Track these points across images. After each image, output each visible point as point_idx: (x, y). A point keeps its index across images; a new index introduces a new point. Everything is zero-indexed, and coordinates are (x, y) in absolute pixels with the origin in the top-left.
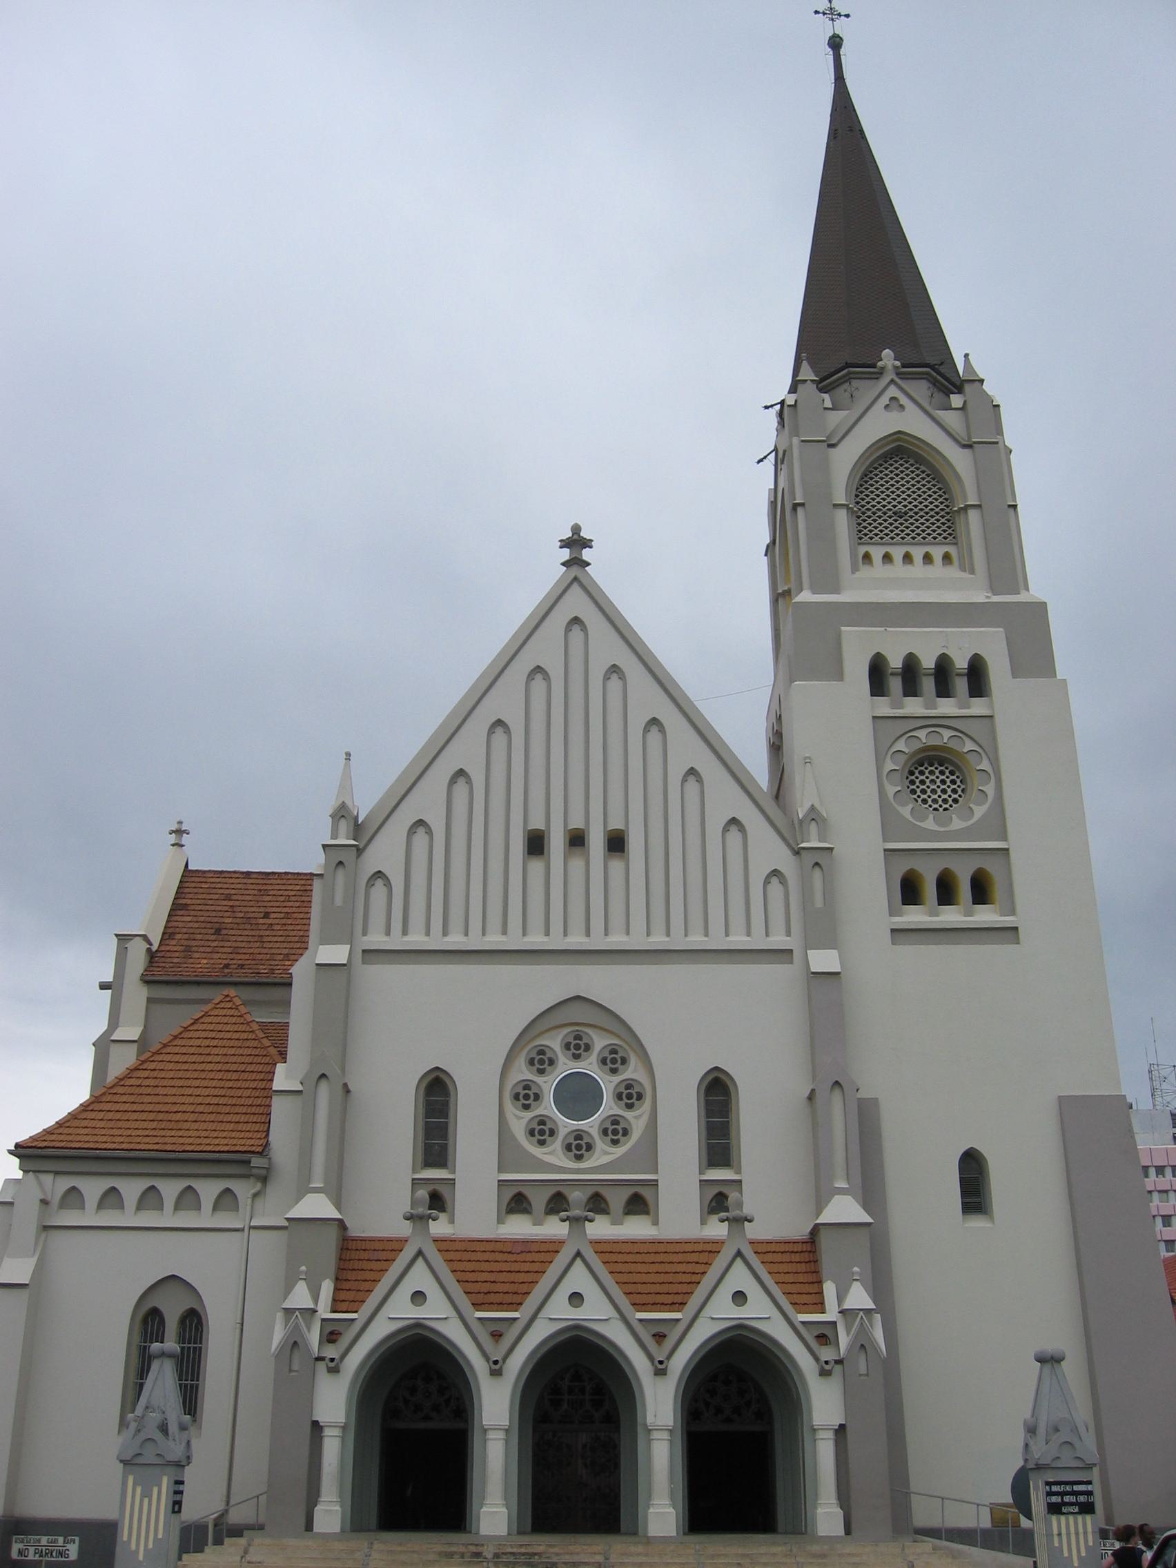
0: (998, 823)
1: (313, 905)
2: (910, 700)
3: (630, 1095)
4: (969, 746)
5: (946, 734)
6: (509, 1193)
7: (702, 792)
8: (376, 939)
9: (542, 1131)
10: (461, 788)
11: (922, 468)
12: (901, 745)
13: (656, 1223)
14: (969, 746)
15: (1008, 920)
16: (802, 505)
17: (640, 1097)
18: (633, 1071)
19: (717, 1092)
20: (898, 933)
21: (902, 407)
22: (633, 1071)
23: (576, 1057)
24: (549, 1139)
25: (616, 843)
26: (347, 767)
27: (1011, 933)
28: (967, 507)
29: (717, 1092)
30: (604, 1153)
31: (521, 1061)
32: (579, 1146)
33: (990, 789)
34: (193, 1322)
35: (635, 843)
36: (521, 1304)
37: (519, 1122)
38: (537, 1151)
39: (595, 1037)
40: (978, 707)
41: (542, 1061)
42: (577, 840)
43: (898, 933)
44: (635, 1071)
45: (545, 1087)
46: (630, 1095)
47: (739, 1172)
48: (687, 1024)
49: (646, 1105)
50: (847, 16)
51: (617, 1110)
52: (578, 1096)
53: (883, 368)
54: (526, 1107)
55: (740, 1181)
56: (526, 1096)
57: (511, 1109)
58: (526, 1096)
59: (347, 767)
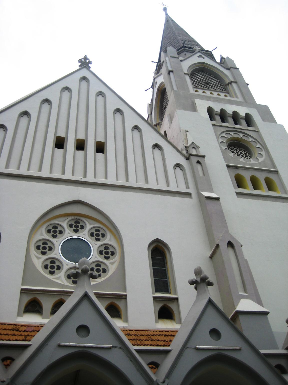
3: (107, 252)
4: (251, 139)
5: (241, 135)
6: (27, 299)
9: (52, 267)
10: (24, 120)
11: (212, 76)
12: (224, 135)
13: (126, 321)
14: (251, 139)
16: (172, 71)
17: (113, 253)
18: (109, 240)
19: (159, 253)
20: (238, 194)
22: (109, 240)
23: (76, 231)
24: (56, 271)
31: (43, 230)
36: (38, 331)
37: (38, 261)
38: (50, 277)
39: (88, 224)
41: (55, 231)
42: (81, 146)
44: (110, 240)
45: (56, 244)
46: (107, 252)
48: (138, 220)
49: (116, 258)
50: (165, 9)
51: (100, 258)
52: (75, 249)
53: (195, 50)
54: (44, 253)
56: (44, 247)
57: (34, 253)
58: (44, 247)
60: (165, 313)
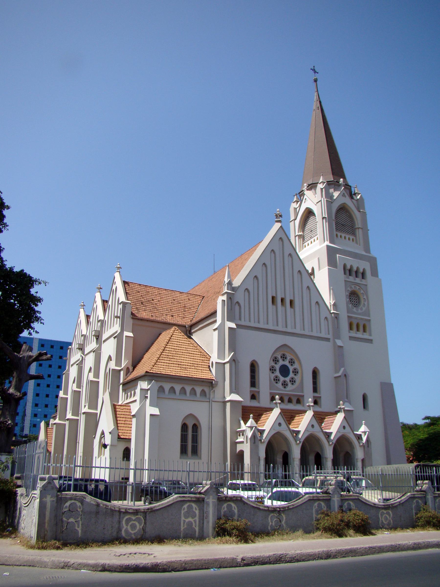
0: (367, 313)
1: (334, 424)
2: (350, 277)
5: (358, 287)
7: (310, 293)
8: (242, 323)
14: (362, 292)
15: (370, 338)
19: (315, 373)
21: (345, 196)
25: (291, 302)
26: (255, 441)
27: (370, 341)
28: (359, 228)
29: (315, 373)
30: (290, 387)
32: (285, 384)
33: (366, 303)
34: (196, 427)
35: (297, 303)
40: (363, 282)
43: (351, 338)
47: (320, 394)
55: (320, 397)
59: (255, 441)
60: (253, 397)
